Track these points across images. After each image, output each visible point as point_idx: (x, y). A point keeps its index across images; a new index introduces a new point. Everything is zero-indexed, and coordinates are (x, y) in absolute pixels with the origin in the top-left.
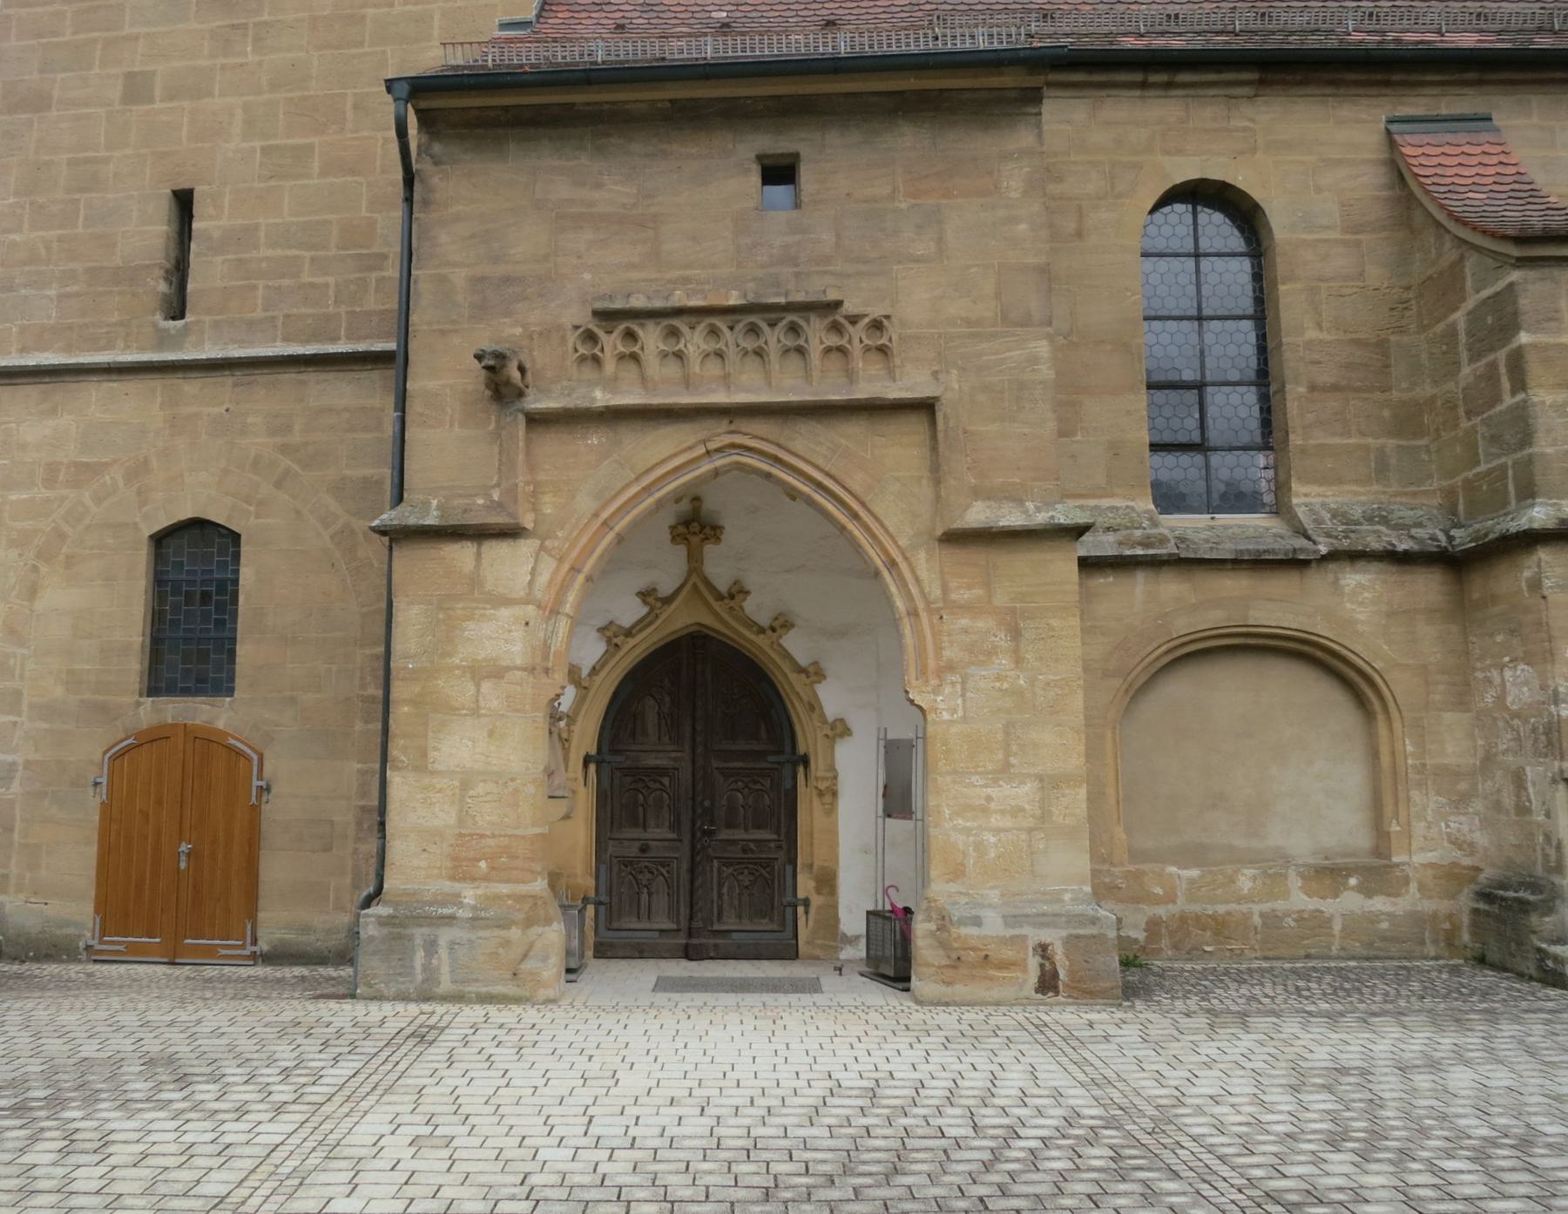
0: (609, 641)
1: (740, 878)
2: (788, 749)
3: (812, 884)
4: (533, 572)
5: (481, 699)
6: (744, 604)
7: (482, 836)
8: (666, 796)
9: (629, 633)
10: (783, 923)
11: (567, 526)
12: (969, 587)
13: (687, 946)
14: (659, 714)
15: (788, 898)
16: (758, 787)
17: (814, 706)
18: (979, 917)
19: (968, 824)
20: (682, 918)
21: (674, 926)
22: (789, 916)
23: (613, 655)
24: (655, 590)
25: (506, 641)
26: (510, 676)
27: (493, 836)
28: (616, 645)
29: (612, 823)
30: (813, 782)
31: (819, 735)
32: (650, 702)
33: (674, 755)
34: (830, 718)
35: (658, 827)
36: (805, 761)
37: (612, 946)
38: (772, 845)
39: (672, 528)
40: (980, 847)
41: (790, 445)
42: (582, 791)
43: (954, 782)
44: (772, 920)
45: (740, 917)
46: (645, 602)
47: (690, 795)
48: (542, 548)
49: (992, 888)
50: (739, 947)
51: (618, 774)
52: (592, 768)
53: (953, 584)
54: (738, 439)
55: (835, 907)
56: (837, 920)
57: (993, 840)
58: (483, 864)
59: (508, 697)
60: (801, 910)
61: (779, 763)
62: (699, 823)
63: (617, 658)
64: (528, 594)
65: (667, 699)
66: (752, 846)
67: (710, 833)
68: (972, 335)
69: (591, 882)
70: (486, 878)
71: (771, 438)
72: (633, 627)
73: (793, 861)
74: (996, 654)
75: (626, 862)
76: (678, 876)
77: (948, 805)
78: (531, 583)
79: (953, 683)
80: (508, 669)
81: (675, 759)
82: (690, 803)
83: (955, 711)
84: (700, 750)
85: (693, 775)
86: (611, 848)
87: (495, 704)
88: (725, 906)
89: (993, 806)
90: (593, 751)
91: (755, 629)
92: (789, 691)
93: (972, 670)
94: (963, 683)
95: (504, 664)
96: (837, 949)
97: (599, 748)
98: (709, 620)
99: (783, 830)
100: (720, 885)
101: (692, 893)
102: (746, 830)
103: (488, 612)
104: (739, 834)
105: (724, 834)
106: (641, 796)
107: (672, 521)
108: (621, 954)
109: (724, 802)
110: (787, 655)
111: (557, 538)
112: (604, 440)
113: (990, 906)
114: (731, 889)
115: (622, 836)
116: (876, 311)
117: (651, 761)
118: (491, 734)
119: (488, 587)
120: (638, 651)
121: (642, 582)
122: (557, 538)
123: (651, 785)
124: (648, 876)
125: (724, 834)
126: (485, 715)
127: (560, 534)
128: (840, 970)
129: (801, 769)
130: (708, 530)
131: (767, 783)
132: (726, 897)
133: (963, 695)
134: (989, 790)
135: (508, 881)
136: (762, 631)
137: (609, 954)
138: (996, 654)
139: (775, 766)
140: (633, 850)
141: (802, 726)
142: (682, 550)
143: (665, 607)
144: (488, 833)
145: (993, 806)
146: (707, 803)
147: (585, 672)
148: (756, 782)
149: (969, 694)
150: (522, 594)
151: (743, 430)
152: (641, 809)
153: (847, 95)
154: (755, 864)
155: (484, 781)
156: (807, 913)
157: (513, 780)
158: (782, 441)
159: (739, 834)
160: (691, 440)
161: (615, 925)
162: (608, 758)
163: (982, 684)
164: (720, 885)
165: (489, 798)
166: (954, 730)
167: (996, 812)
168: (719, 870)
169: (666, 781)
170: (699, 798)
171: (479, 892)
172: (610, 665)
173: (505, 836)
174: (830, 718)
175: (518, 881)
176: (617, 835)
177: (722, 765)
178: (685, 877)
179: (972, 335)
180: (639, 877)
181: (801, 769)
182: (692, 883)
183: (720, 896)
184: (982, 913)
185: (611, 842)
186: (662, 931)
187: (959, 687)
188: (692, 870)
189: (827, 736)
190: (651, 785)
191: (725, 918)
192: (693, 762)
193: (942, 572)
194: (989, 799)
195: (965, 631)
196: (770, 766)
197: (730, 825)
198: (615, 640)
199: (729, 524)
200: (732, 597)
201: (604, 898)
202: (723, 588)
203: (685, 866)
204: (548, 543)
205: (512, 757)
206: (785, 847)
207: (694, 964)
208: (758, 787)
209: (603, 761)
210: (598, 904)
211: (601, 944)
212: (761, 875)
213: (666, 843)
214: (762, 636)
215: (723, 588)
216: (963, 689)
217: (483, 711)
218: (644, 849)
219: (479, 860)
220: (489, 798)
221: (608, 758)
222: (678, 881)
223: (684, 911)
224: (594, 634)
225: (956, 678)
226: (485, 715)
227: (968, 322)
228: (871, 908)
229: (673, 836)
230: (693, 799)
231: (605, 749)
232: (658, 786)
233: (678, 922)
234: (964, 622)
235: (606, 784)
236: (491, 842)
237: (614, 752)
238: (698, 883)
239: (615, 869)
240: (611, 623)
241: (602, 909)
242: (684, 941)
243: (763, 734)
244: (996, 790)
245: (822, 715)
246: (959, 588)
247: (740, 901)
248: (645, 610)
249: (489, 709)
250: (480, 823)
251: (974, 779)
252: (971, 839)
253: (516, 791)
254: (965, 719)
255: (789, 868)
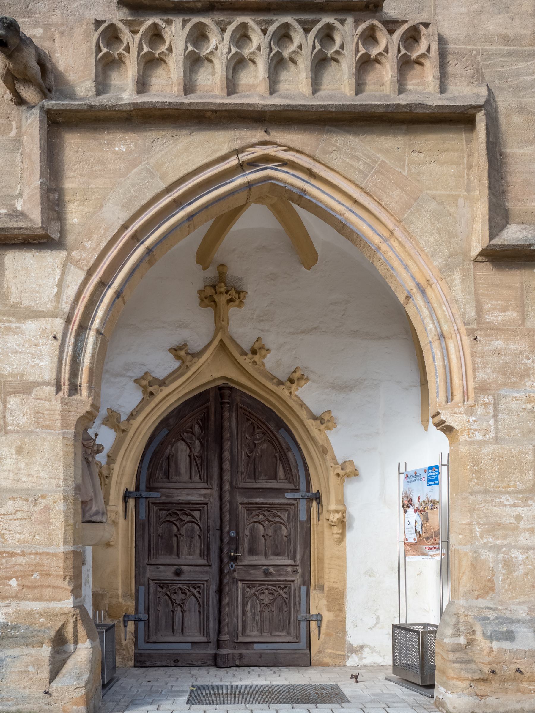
0: (144, 392)
1: (262, 597)
2: (303, 486)
3: (324, 602)
4: (60, 284)
5: (8, 414)
6: (265, 361)
7: (12, 554)
8: (196, 526)
9: (163, 383)
10: (298, 636)
11: (96, 237)
12: (504, 309)
13: (215, 656)
14: (190, 456)
15: (303, 614)
16: (277, 519)
17: (324, 450)
18: (512, 632)
19: (498, 542)
20: (211, 631)
21: (204, 639)
22: (303, 631)
23: (148, 403)
24: (185, 345)
25: (33, 355)
26: (37, 391)
27: (23, 554)
28: (151, 394)
29: (149, 551)
30: (324, 516)
31: (332, 474)
32: (181, 446)
33: (204, 492)
34: (340, 461)
35: (190, 554)
36: (318, 498)
37: (149, 656)
38: (289, 569)
39: (200, 292)
40: (508, 564)
41: (326, 159)
42: (121, 521)
43: (485, 501)
44: (289, 633)
45: (261, 631)
46: (178, 357)
47: (218, 527)
48: (68, 259)
49: (520, 604)
50: (261, 655)
51: (154, 509)
52: (131, 503)
53: (487, 306)
54: (271, 150)
55: (343, 622)
56: (344, 631)
57: (521, 557)
58: (13, 583)
59: (36, 412)
60: (313, 624)
61: (295, 499)
62: (226, 550)
63: (152, 405)
64: (56, 307)
65: (197, 443)
66: (272, 570)
67: (234, 559)
68: (510, 54)
69: (131, 604)
70: (16, 597)
71: (307, 150)
72: (167, 378)
73: (307, 583)
74: (529, 376)
75: (162, 585)
76: (208, 595)
77: (479, 524)
78: (58, 295)
79: (485, 405)
80: (37, 384)
81: (204, 496)
82: (218, 533)
83: (487, 431)
84: (227, 487)
85: (221, 509)
86: (150, 572)
87: (23, 420)
88: (248, 621)
89: (522, 525)
90: (132, 488)
91: (275, 381)
92: (304, 437)
93: (504, 391)
94: (496, 405)
95: (31, 379)
96: (344, 657)
97: (137, 488)
98: (233, 374)
99: (299, 557)
100: (244, 604)
101: (220, 611)
102: (266, 556)
103: (13, 325)
104: (260, 560)
105: (248, 560)
106: (174, 527)
107: (200, 285)
108: (158, 663)
109: (247, 533)
110: (302, 405)
111: (84, 249)
112: (132, 146)
113: (518, 621)
114: (253, 607)
115: (159, 562)
116: (414, 19)
117: (183, 497)
118: (19, 451)
119: (12, 299)
120: (172, 399)
121: (175, 341)
122: (84, 249)
123: (184, 518)
124: (182, 596)
125: (248, 560)
126: (12, 432)
127: (87, 245)
128: (356, 677)
129: (314, 504)
130: (233, 292)
131: (284, 516)
132: (249, 614)
133: (495, 416)
134: (519, 509)
135: (40, 599)
136: (280, 383)
137: (148, 664)
138: (529, 376)
139: (292, 502)
140: (168, 574)
141: (316, 469)
142: (209, 312)
143: (195, 359)
144: (18, 551)
145: (522, 525)
146: (233, 534)
147: (124, 418)
148: (275, 516)
149: (500, 416)
150: (49, 306)
151: (278, 141)
152: (175, 539)
153: (174, 654)
154: (274, 585)
155: (13, 499)
156: (319, 627)
157: (43, 497)
158: (318, 154)
159: (260, 560)
160: (225, 149)
161: (153, 638)
162: (145, 494)
163: (514, 405)
164: (244, 604)
165: (19, 515)
166: (486, 450)
167: (525, 530)
168: (243, 590)
169: (196, 514)
170: (227, 529)
171: (10, 610)
172: (148, 409)
173: (36, 554)
174: (340, 461)
175: (53, 599)
176: (152, 561)
177: (246, 500)
178: (213, 596)
179: (510, 54)
180: (173, 597)
181: (314, 504)
182: (220, 601)
183: (244, 613)
184: (513, 628)
185: (148, 566)
186: (193, 643)
187: (491, 409)
188: (220, 591)
189: (338, 475)
190: (184, 518)
191: (248, 631)
192: (221, 498)
193: (476, 294)
194: (518, 518)
195: (498, 353)
196: (286, 501)
197: (252, 551)
198: (151, 389)
199: (250, 289)
200: (254, 352)
201: (143, 616)
202: (246, 346)
203: (214, 587)
204: (74, 254)
205: (42, 474)
206: (300, 570)
207: (222, 672)
208: (277, 519)
209: (141, 497)
210: (137, 621)
211: (140, 655)
212: (280, 595)
213: (197, 568)
214: (282, 387)
215: (246, 346)
216: (496, 410)
217: (10, 428)
218: (178, 573)
219: (9, 578)
220: (19, 515)
221: (145, 494)
222: (208, 601)
223: (213, 625)
224: (132, 384)
225: (489, 399)
226: (12, 432)
227: (506, 40)
228: (396, 622)
229: (204, 562)
230: (221, 529)
231: (143, 486)
232: (189, 518)
233: (208, 636)
234: (498, 344)
235: (143, 516)
236: (22, 560)
237: (150, 489)
238: (226, 600)
239: (152, 591)
240: (146, 373)
241: (141, 625)
242: (213, 652)
243: (281, 473)
244: (525, 509)
245: (334, 458)
246: (494, 309)
247: (261, 617)
248: (177, 364)
249: (17, 425)
250: (10, 541)
251: (504, 498)
252: (501, 556)
253: (47, 508)
254: (496, 440)
255: (304, 589)
